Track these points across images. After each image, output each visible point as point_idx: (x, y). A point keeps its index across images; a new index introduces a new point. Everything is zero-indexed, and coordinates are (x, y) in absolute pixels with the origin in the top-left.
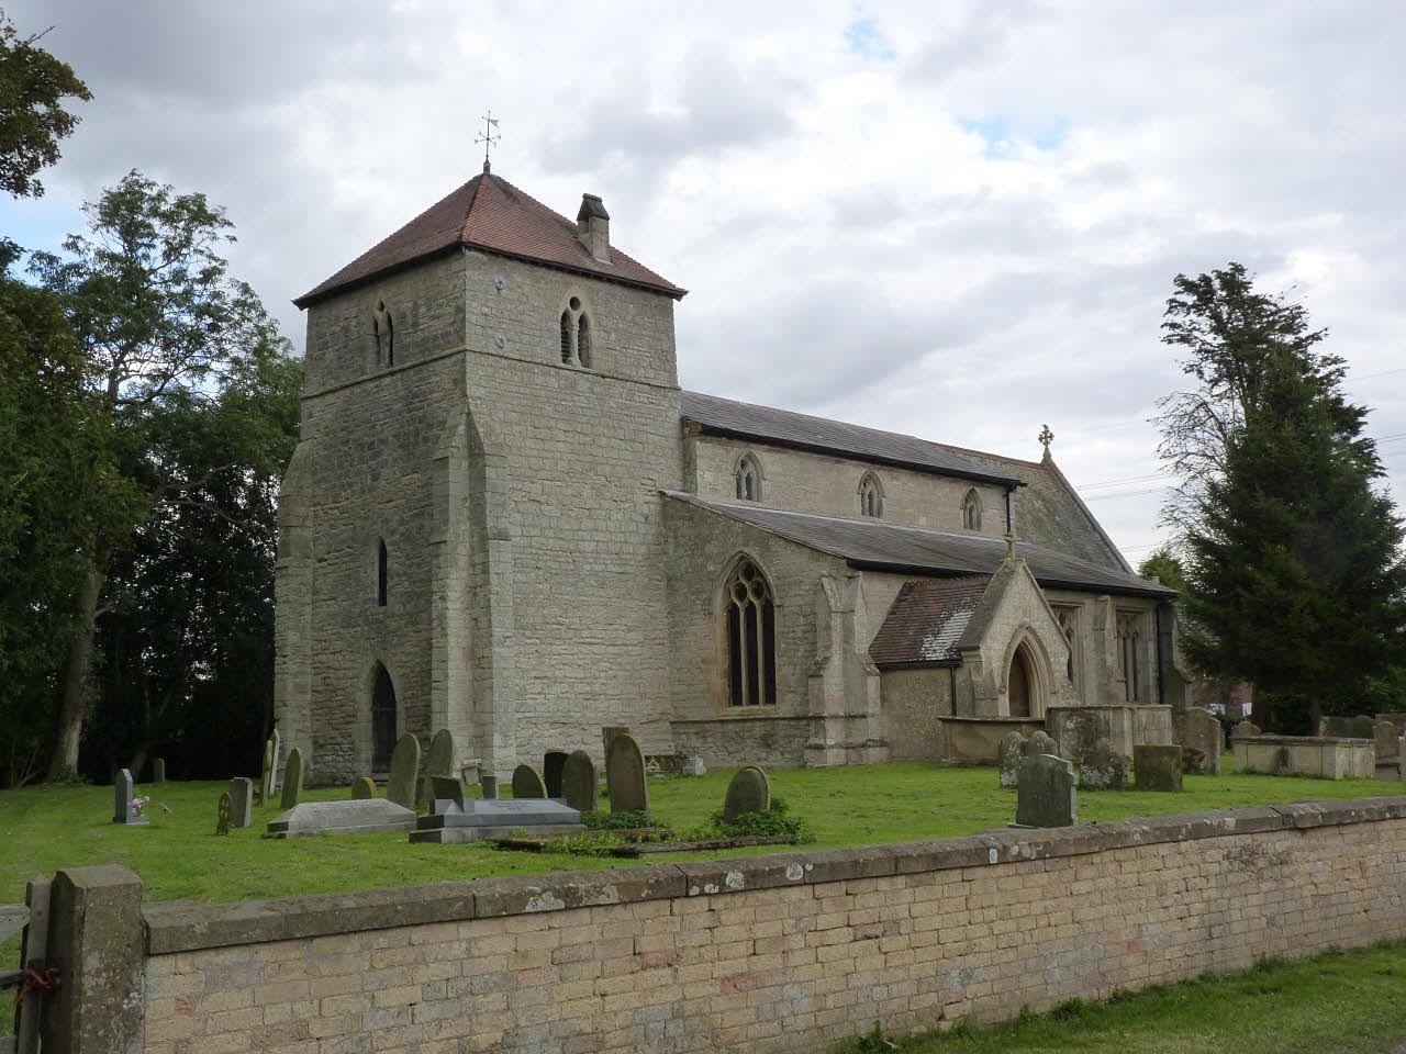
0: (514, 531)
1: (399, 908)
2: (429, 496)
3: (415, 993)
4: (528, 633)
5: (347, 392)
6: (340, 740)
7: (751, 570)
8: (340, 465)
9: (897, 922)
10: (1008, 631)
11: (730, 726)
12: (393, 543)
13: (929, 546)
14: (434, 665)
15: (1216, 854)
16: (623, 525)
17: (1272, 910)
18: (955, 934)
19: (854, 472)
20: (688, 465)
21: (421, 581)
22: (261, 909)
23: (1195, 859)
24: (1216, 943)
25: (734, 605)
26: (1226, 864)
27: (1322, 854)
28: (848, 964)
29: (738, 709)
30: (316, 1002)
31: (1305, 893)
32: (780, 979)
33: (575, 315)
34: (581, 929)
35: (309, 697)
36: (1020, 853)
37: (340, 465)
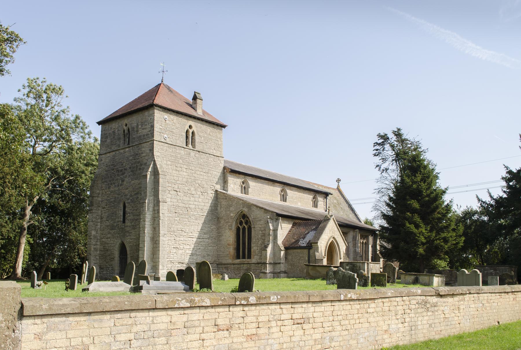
0: (168, 200)
1: (126, 303)
2: (141, 187)
3: (131, 336)
4: (172, 233)
5: (114, 153)
6: (108, 266)
7: (244, 216)
8: (111, 177)
9: (309, 318)
10: (327, 238)
11: (237, 265)
12: (128, 203)
13: (303, 212)
14: (140, 243)
15: (414, 302)
16: (204, 203)
17: (431, 322)
18: (329, 324)
19: (278, 189)
20: (225, 182)
21: (137, 215)
22: (70, 301)
23: (408, 303)
24: (413, 332)
25: (239, 227)
26: (417, 305)
27: (447, 304)
28: (291, 333)
29: (239, 260)
30: (92, 338)
31: (441, 317)
32: (267, 337)
33: (191, 131)
34: (196, 315)
35: (98, 252)
36: (351, 297)
37: (111, 177)
